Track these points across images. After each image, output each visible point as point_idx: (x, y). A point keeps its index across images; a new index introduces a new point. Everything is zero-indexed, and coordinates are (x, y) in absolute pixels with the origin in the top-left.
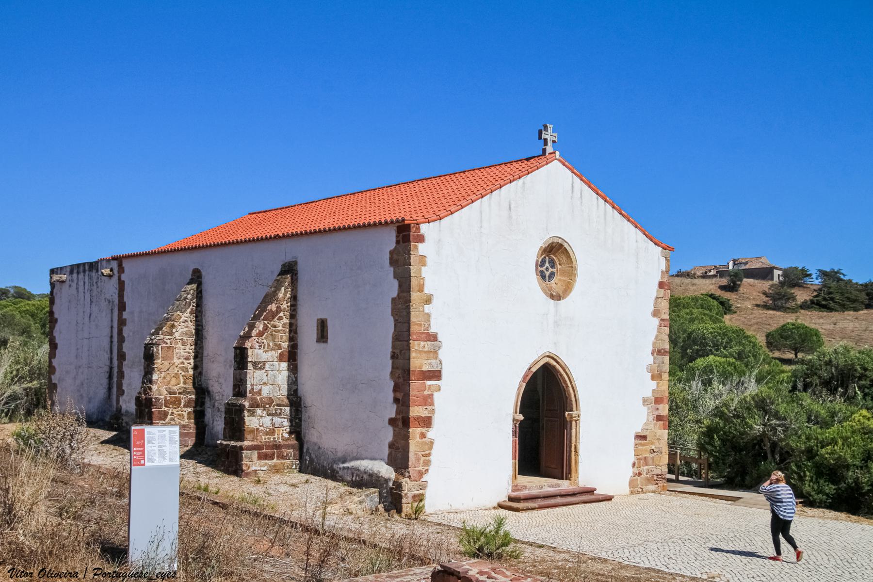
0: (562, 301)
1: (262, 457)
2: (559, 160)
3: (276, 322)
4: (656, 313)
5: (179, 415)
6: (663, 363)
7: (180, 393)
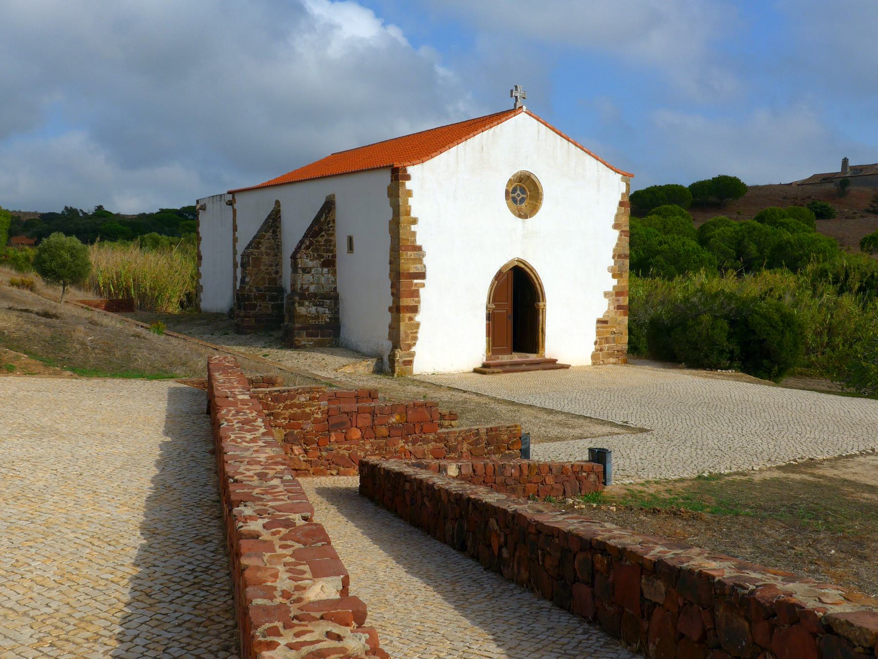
0: (529, 220)
1: (308, 335)
2: (526, 112)
3: (319, 239)
4: (616, 226)
5: (265, 307)
6: (624, 264)
7: (265, 291)
